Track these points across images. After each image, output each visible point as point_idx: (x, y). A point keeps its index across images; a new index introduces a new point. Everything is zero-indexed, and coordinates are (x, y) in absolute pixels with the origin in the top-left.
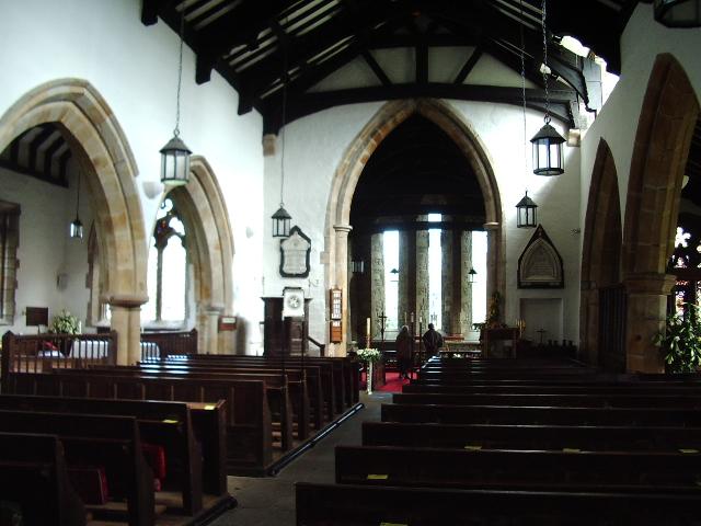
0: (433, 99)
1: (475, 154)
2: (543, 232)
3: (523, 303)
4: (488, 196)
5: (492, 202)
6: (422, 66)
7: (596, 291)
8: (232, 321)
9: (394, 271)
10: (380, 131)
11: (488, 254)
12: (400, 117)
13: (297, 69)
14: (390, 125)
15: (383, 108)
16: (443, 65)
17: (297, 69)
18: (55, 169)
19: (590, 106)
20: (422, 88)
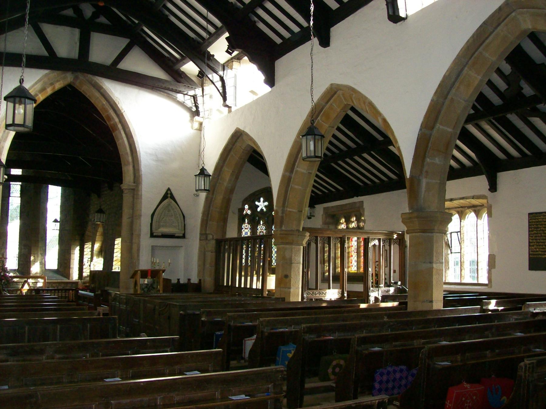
0: (90, 76)
1: (120, 126)
2: (171, 194)
3: (153, 248)
4: (128, 162)
5: (131, 168)
6: (84, 46)
7: (214, 242)
8: (287, 256)
9: (56, 221)
10: (40, 95)
11: (61, 206)
12: (58, 86)
13: (333, 164)
14: (49, 91)
15: (46, 75)
16: (103, 49)
17: (333, 164)
18: (532, 244)
19: (228, 103)
20: (82, 64)
